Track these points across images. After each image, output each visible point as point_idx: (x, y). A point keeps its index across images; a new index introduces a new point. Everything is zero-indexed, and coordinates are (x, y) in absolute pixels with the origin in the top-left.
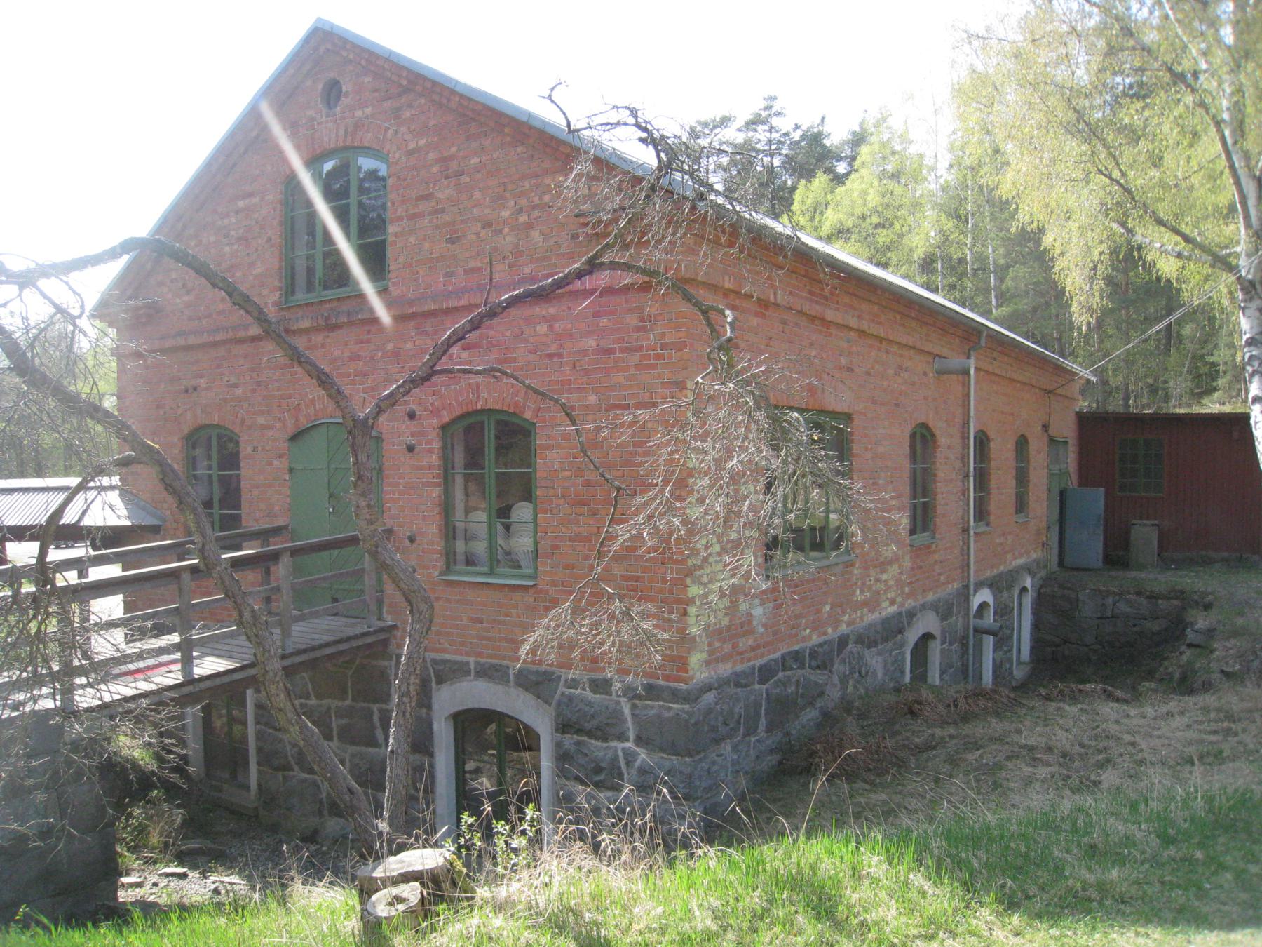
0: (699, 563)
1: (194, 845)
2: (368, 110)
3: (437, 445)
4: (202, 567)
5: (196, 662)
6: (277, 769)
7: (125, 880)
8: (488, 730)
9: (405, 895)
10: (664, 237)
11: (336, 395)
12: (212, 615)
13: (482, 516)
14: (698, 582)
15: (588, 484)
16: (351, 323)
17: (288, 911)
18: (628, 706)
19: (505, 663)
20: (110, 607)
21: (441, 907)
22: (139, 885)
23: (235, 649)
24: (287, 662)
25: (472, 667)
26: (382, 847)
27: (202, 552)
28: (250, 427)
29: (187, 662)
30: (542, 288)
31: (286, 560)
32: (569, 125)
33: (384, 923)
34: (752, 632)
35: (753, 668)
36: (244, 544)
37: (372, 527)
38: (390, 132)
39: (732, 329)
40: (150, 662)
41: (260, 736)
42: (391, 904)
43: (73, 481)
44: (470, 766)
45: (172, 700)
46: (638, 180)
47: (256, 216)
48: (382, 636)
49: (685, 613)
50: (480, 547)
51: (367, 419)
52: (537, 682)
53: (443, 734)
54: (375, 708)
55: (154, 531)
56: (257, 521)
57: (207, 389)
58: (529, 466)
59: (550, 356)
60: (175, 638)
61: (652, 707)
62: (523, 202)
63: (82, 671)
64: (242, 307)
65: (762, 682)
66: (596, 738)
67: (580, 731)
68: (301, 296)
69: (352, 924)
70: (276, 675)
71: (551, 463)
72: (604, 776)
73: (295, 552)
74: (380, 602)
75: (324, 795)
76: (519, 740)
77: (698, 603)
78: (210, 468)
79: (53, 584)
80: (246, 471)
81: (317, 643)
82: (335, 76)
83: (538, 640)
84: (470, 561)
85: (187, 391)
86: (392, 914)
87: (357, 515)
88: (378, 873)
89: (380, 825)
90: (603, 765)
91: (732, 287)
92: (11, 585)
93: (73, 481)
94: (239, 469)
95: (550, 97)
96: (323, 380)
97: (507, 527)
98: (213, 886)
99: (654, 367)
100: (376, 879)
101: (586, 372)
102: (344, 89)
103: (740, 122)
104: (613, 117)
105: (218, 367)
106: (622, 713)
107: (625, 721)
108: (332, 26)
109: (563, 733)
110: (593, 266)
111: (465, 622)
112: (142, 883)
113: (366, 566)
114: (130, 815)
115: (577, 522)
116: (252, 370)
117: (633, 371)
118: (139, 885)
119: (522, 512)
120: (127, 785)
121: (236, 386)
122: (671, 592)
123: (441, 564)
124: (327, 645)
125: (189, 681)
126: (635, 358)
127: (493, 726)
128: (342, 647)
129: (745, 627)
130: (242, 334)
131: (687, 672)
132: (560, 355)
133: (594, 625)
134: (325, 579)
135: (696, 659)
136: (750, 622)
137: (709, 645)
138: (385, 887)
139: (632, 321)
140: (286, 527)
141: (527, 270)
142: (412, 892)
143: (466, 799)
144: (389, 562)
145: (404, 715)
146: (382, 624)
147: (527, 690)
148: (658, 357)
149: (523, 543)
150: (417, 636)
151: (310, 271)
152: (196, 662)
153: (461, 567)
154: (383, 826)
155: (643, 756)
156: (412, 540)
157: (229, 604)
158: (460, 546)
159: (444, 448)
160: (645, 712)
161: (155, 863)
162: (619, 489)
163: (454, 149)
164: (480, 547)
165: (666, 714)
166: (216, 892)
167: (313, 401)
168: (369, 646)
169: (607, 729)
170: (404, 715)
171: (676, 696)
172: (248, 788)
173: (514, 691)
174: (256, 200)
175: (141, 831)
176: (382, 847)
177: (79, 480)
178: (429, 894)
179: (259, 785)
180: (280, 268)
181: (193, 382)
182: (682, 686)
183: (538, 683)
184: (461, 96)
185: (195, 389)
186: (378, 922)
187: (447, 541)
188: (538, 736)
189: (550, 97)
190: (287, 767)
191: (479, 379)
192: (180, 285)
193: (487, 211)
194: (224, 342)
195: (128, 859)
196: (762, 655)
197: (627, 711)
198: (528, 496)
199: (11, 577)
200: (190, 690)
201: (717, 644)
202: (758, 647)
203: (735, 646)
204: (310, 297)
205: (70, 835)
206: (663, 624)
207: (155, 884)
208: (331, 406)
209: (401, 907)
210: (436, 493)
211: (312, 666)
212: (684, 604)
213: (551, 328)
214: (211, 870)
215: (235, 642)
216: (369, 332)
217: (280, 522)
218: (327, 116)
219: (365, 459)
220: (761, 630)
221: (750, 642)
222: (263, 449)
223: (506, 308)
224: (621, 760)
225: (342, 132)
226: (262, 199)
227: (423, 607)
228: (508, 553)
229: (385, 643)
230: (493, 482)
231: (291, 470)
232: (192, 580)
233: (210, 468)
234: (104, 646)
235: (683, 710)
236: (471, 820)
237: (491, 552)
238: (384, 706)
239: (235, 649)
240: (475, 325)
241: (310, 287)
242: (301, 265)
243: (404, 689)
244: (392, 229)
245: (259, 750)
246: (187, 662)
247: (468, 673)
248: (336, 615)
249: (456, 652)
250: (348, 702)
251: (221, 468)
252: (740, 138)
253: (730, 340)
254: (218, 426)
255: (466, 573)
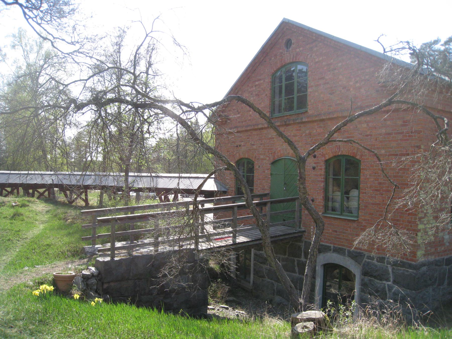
0: (423, 216)
1: (231, 298)
2: (301, 49)
3: (323, 167)
4: (246, 205)
5: (237, 237)
6: (260, 277)
7: (209, 307)
8: (335, 272)
9: (308, 326)
10: (420, 90)
11: (294, 148)
12: (245, 221)
13: (339, 194)
14: (422, 223)
15: (380, 183)
16: (294, 124)
17: (263, 326)
18: (391, 268)
19: (344, 247)
20: (210, 217)
21: (321, 332)
22: (214, 309)
23: (250, 234)
24: (273, 239)
25: (332, 248)
26: (301, 308)
27: (247, 201)
28: (258, 159)
29: (234, 237)
30: (371, 111)
31: (269, 205)
32: (384, 50)
33: (300, 334)
34: (444, 245)
35: (443, 259)
36: (254, 199)
37: (304, 195)
38: (309, 56)
39: (448, 125)
40: (226, 236)
41: (255, 265)
42: (303, 328)
43: (206, 176)
44: (328, 284)
45: (233, 249)
46: (408, 69)
47: (262, 87)
48: (300, 234)
49: (417, 235)
50: (337, 205)
51: (304, 157)
52: (357, 256)
53: (320, 271)
54: (296, 259)
55: (225, 193)
56: (259, 191)
57: (244, 146)
58: (358, 176)
59: (367, 136)
60: (230, 229)
61: (401, 270)
62: (358, 79)
63: (202, 237)
64: (263, 118)
65: (447, 265)
66: (378, 279)
67: (371, 276)
68: (277, 114)
69: (288, 332)
70: (268, 244)
71: (366, 176)
72: (382, 294)
73: (272, 202)
74: (300, 222)
75: (275, 288)
76: (347, 276)
77: (422, 231)
78: (244, 172)
79: (198, 208)
80: (256, 174)
81: (277, 235)
82: (288, 36)
83: (360, 241)
84: (333, 210)
85: (237, 146)
86: (304, 331)
87: (299, 191)
88: (299, 317)
89: (300, 300)
90: (379, 289)
91: (441, 109)
92: (186, 208)
93: (206, 176)
94: (253, 173)
95: (378, 41)
96: (290, 143)
97: (348, 198)
98: (237, 313)
99: (407, 140)
100: (298, 319)
101: (381, 142)
102: (293, 42)
103: (442, 42)
104: (401, 46)
105: (248, 138)
106: (388, 270)
107: (389, 274)
108: (289, 20)
109: (365, 276)
110: (390, 102)
111: (331, 231)
112: (215, 308)
113: (296, 209)
114: (212, 286)
115: (375, 197)
116: (259, 140)
117: (399, 142)
118: (214, 309)
119: (354, 193)
120: (213, 276)
121: (254, 145)
122: (411, 226)
123: (323, 210)
124: (281, 236)
125: (235, 244)
126: (400, 137)
127: (337, 271)
128: (287, 237)
129: (441, 242)
130: (256, 127)
131: (416, 257)
132: (371, 135)
133: (384, 236)
134: (281, 213)
135: (420, 253)
136: (443, 241)
137: (426, 248)
138: (301, 322)
139: (400, 122)
140: (268, 194)
141: (359, 104)
142: (311, 325)
143: (325, 296)
144: (310, 208)
145: (311, 262)
146: (300, 230)
147: (352, 258)
148: (410, 136)
149: (354, 204)
150: (318, 235)
151: (280, 106)
152: (237, 237)
153: (330, 212)
154: (301, 301)
155: (396, 287)
156: (313, 201)
157: (254, 219)
158: (330, 204)
159: (326, 168)
160: (397, 271)
161: (218, 303)
162: (396, 186)
163: (332, 61)
164: (337, 205)
165: (406, 273)
166: (238, 315)
167: (280, 151)
168: (296, 237)
169: (383, 276)
170: (311, 262)
171: (410, 266)
172: (250, 282)
173: (347, 258)
174: (262, 82)
175: (215, 291)
176: (301, 308)
177: (208, 175)
178: (316, 327)
179: (253, 281)
180: (270, 105)
181: (239, 144)
182: (413, 263)
183: (357, 256)
184: (335, 41)
185: (240, 146)
186: (298, 334)
187: (325, 202)
188: (355, 275)
189: (378, 41)
190: (263, 277)
191: (340, 144)
192: (236, 111)
193: (344, 83)
194: (250, 130)
195: (210, 300)
196: (447, 255)
197: (390, 270)
198: (356, 187)
199: (186, 205)
200: (236, 247)
201: (429, 248)
202: (446, 251)
203: (436, 249)
204: (280, 115)
205: (199, 289)
206: (410, 238)
207: (218, 310)
208: (291, 152)
209: (306, 330)
210: (322, 185)
211: (277, 242)
212: (416, 231)
213: (368, 125)
214: (237, 308)
215: (250, 232)
216: (300, 126)
217: (266, 192)
218: (287, 52)
219: (303, 171)
220: (447, 244)
221: (443, 249)
222: (262, 167)
223: (356, 118)
224: (387, 288)
225: (292, 57)
226: (264, 81)
227: (321, 224)
228: (348, 208)
229: (301, 237)
230: (344, 181)
231: (271, 174)
232: (238, 210)
233: (244, 172)
234: (209, 229)
235: (413, 272)
236: (331, 303)
237: (341, 206)
238: (299, 259)
239: (250, 234)
240: (345, 124)
241: (280, 111)
242: (277, 103)
243: (312, 253)
244: (309, 90)
245: (254, 270)
246: (234, 237)
247: (330, 250)
248: (284, 225)
249: (327, 242)
250: (287, 256)
251: (247, 173)
252: (442, 48)
253: (446, 130)
254: (247, 159)
255: (332, 214)
